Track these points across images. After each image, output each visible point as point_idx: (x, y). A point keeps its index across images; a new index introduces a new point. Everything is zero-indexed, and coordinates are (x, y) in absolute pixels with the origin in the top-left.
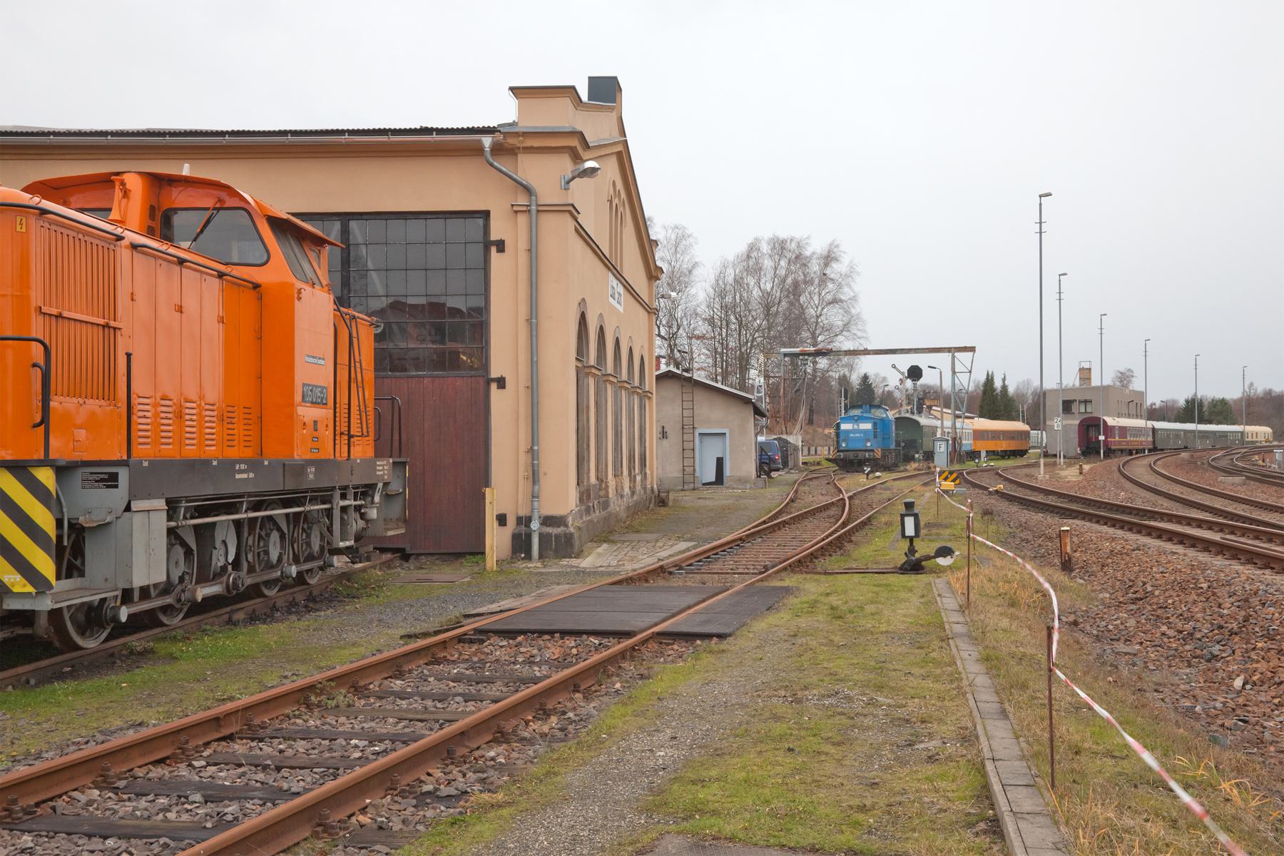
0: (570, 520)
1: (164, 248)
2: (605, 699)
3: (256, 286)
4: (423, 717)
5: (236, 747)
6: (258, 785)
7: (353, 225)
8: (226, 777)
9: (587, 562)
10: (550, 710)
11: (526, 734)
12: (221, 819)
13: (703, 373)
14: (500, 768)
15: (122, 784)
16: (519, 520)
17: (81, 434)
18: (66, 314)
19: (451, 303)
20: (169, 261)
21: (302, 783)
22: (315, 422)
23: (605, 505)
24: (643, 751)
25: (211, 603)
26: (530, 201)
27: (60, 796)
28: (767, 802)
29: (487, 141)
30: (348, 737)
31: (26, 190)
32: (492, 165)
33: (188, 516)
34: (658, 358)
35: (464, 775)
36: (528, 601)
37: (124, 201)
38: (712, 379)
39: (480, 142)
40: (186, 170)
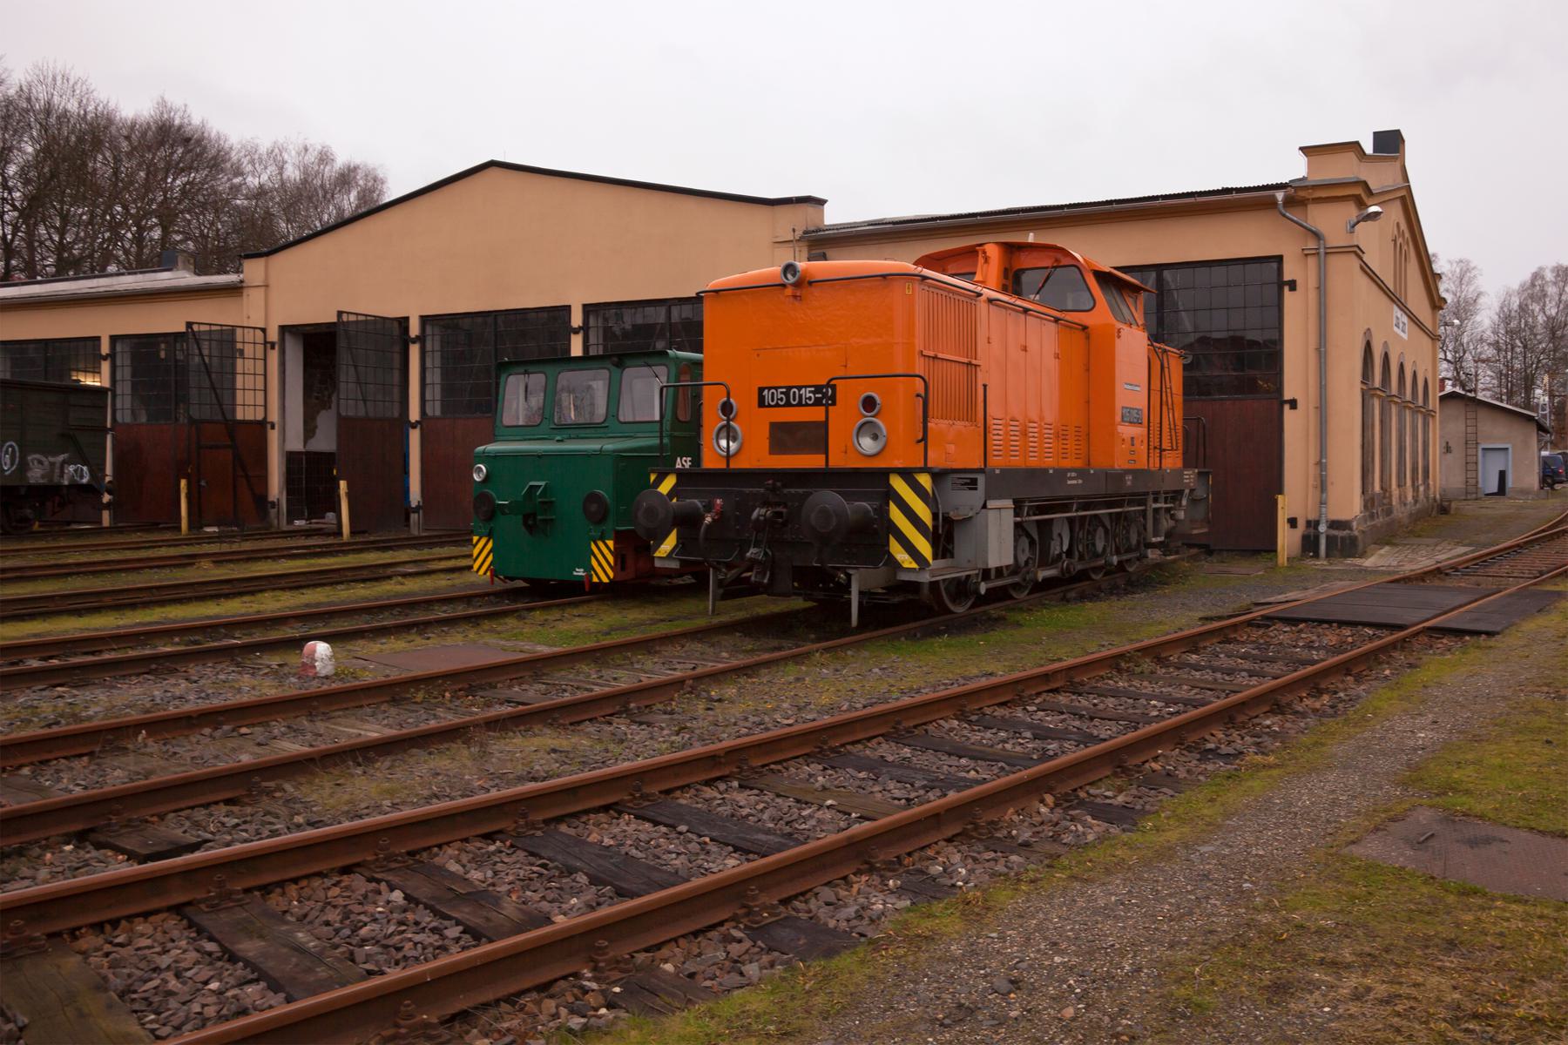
0: (1355, 524)
1: (1012, 301)
2: (1375, 683)
3: (1085, 328)
4: (1212, 687)
5: (1061, 698)
6: (1075, 730)
7: (1167, 274)
8: (1051, 721)
9: (1369, 562)
10: (1323, 689)
11: (1300, 709)
12: (1044, 754)
13: (1488, 393)
14: (1274, 736)
15: (974, 718)
16: (1309, 523)
17: (952, 448)
18: (940, 355)
19: (1250, 336)
20: (1017, 311)
21: (1109, 732)
22: (1132, 438)
23: (1389, 512)
24: (1405, 732)
25: (1049, 584)
26: (1319, 245)
27: (931, 722)
28: (1519, 788)
29: (1280, 196)
30: (1150, 698)
31: (916, 263)
32: (1284, 216)
33: (1031, 513)
34: (1443, 380)
35: (1243, 738)
36: (1311, 594)
37: (985, 265)
38: (1497, 399)
39: (1274, 196)
40: (1031, 238)
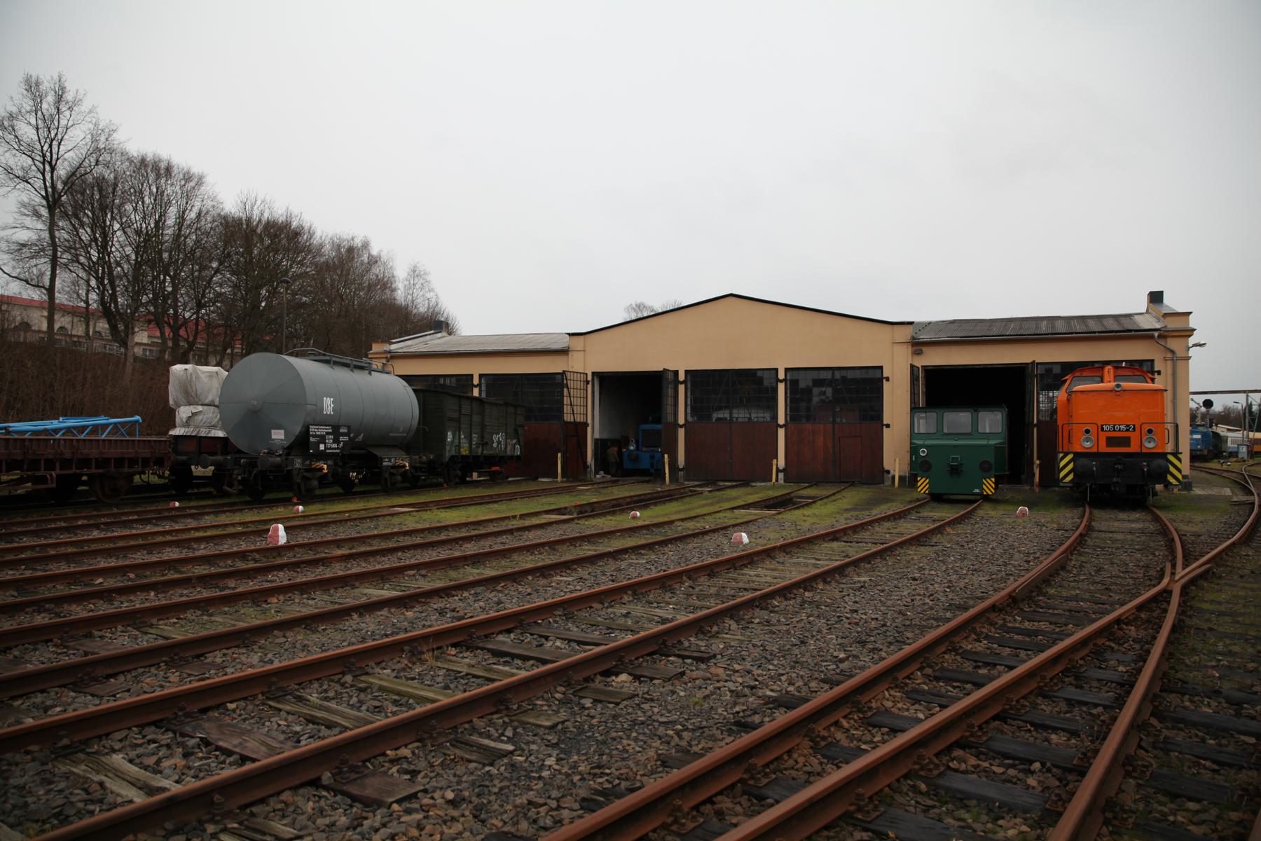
29: (1156, 334)
